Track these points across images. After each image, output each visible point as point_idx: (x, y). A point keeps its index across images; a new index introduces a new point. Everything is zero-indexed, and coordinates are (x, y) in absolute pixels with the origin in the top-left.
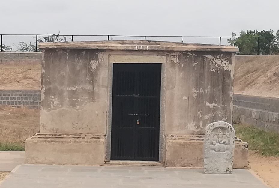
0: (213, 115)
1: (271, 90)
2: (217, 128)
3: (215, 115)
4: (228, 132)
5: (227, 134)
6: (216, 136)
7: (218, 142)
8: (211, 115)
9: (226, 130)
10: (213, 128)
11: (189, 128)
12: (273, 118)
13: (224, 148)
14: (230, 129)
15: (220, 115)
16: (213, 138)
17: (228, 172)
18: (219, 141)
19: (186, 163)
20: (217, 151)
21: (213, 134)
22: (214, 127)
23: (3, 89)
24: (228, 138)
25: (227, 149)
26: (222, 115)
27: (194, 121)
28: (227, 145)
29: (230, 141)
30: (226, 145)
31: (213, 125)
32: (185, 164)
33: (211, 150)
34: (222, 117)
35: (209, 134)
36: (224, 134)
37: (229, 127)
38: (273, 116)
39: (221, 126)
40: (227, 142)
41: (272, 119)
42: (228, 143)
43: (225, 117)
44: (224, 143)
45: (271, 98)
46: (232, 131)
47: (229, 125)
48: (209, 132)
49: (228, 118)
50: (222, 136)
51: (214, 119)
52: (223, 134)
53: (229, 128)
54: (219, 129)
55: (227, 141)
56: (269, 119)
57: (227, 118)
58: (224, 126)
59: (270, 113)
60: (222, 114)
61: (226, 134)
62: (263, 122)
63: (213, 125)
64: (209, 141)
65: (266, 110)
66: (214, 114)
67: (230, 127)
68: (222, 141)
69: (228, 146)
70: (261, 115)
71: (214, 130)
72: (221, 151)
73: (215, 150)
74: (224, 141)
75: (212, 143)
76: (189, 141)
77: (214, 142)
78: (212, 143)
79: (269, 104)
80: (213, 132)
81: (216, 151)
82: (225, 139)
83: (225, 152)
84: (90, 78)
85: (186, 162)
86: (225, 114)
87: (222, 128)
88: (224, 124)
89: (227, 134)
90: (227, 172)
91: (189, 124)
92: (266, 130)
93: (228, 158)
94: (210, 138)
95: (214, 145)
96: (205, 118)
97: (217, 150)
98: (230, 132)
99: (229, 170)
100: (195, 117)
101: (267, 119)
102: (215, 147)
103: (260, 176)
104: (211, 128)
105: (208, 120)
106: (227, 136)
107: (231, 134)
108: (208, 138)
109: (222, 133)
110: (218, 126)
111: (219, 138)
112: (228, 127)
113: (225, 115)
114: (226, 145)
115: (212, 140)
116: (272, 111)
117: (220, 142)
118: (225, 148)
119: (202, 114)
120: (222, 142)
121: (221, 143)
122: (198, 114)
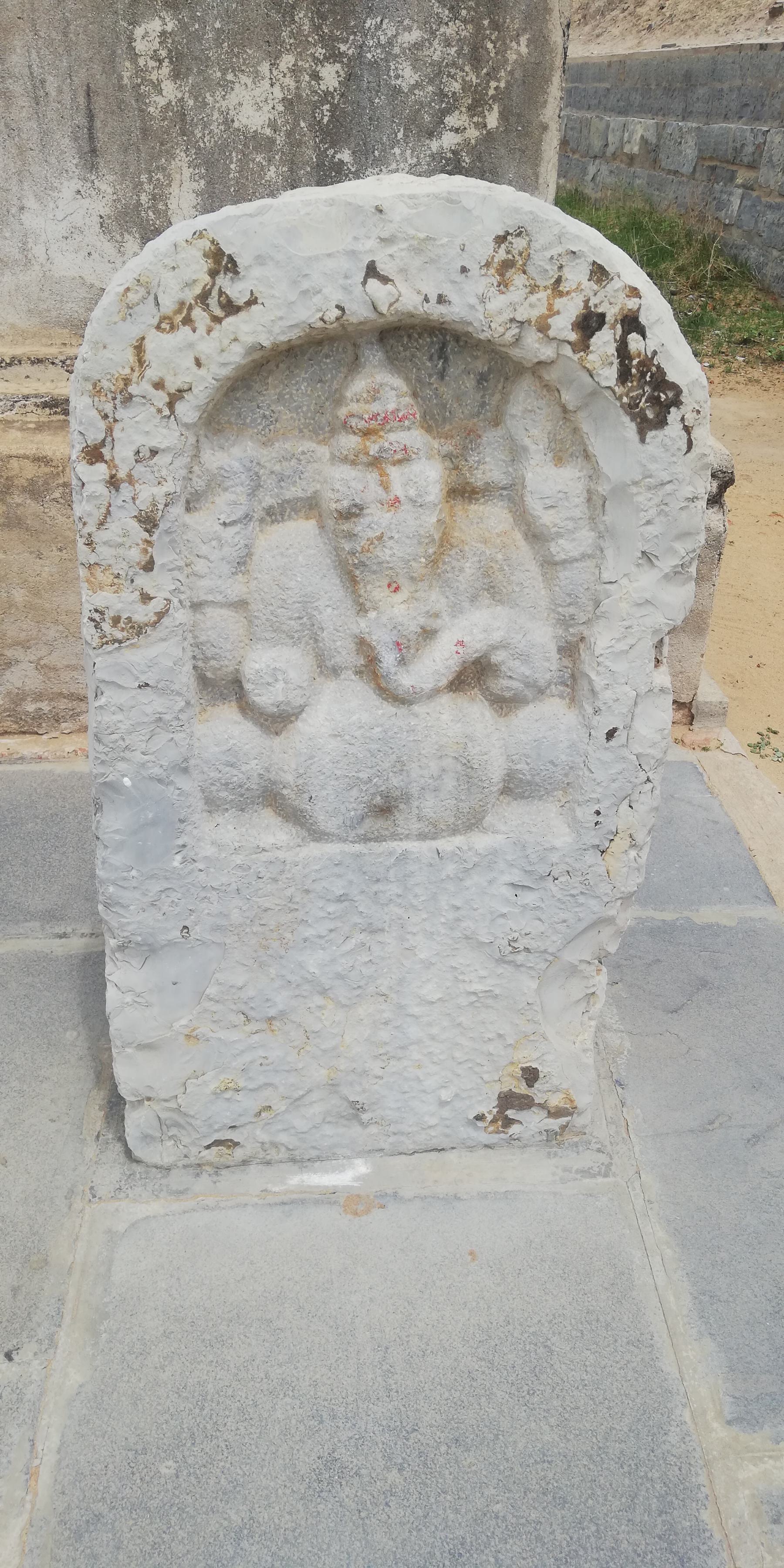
0: (331, 76)
1: (601, 38)
2: (322, 350)
3: (350, 78)
4: (570, 446)
5: (551, 483)
6: (301, 531)
7: (346, 654)
8: (295, 71)
10: (224, 347)
11: (38, 251)
12: (626, 139)
14: (609, 375)
15: (408, 76)
16: (236, 589)
17: (531, 1122)
18: (363, 644)
19: (39, 697)
20: (329, 824)
21: (225, 503)
22: (256, 329)
23: (83, 99)
24: (549, 564)
25: (514, 787)
26: (439, 71)
27: (91, 155)
28: (525, 716)
29: (602, 639)
30: (505, 704)
32: (31, 707)
33: (213, 805)
34: (441, 94)
35: (148, 493)
36: (478, 478)
37: (589, 323)
38: (626, 135)
40: (524, 657)
41: (622, 147)
42: (546, 664)
43: (476, 107)
44: (474, 674)
45: (615, 59)
47: (599, 273)
48: (122, 453)
49: (504, 116)
50: (442, 546)
51: (333, 133)
52: (462, 492)
53: (604, 341)
54: (359, 385)
55: (522, 633)
56: (606, 145)
57: (492, 120)
58: (481, 306)
59: (615, 121)
60: (436, 52)
61: (512, 493)
62: (576, 156)
63: (222, 262)
65: (589, 108)
66: (334, 56)
67: (631, 323)
68: (428, 634)
69: (548, 723)
70: (572, 129)
71: (270, 393)
72: (406, 821)
73: (294, 816)
74: (476, 645)
75: (224, 687)
76: (31, 449)
77: (273, 668)
78: (224, 687)
79: (608, 85)
80: (228, 457)
81: (318, 835)
82: (492, 588)
83: (481, 841)
85: (33, 681)
86: (476, 58)
87: (423, 343)
89: (551, 483)
90: (509, 1122)
91: (31, 202)
92: (589, 190)
93: (536, 927)
94: (159, 584)
95: (276, 721)
96: (228, 122)
97: (329, 806)
98: (615, 442)
99: (538, 1093)
100: (99, 103)
101: (597, 144)
104: (159, 345)
105: (263, 144)
107: (621, 491)
109: (427, 475)
111: (378, 592)
112: (563, 325)
113: (473, 78)
114: (505, 704)
115: (221, 626)
116: (623, 112)
117: (388, 659)
118: (496, 772)
119: (181, 61)
120: (438, 661)
122: (134, 57)
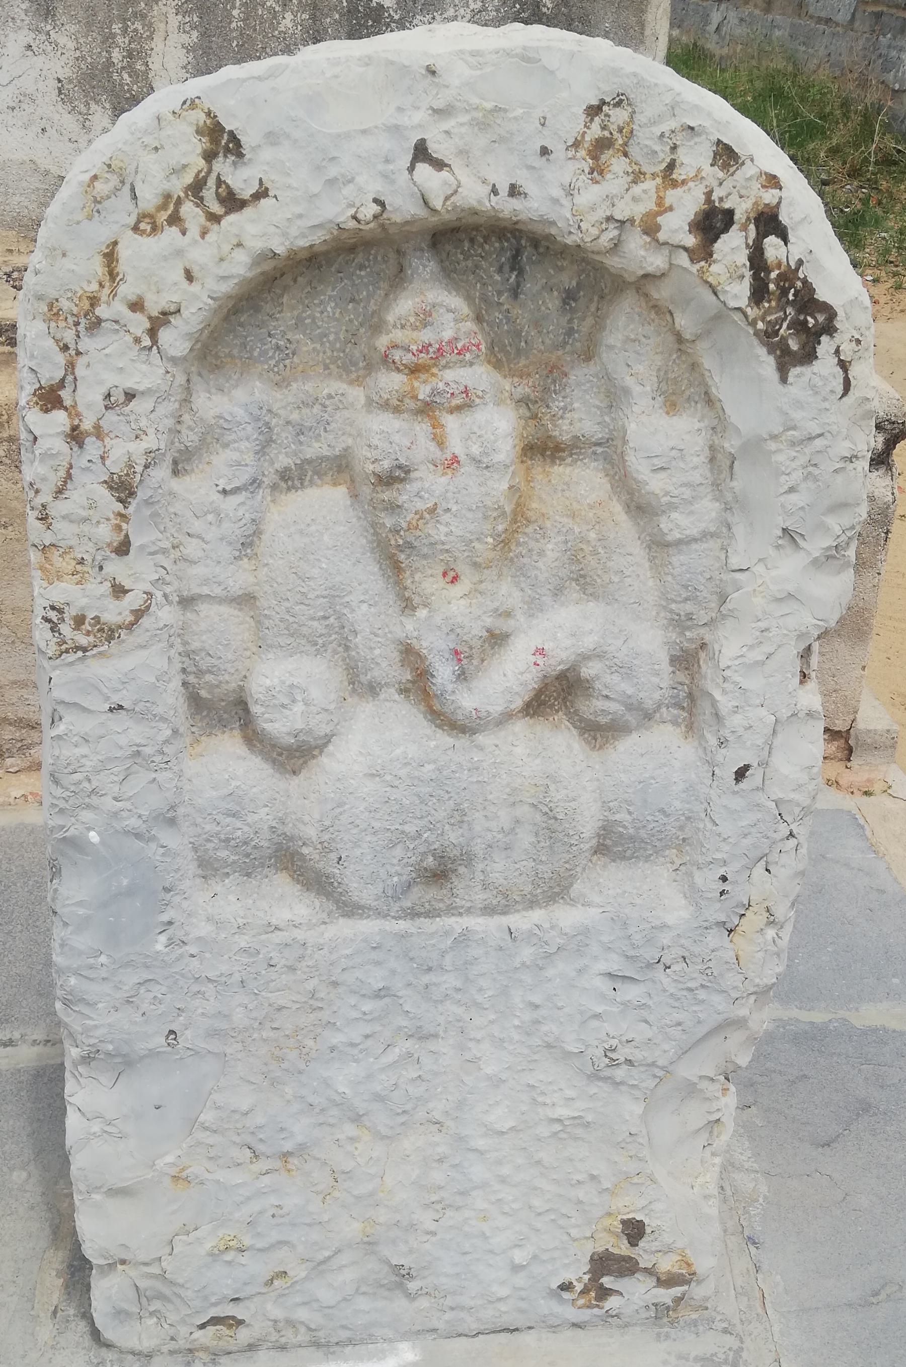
2: (354, 260)
4: (687, 387)
5: (660, 437)
6: (326, 501)
7: (387, 667)
9: (624, 325)
10: (223, 255)
13: (551, 825)
14: (739, 293)
16: (239, 578)
17: (635, 1293)
18: (409, 654)
20: (366, 895)
21: (225, 464)
22: (265, 231)
24: (659, 545)
29: (730, 646)
31: (189, 151)
33: (209, 868)
35: (122, 450)
36: (564, 431)
37: (712, 223)
39: (469, 185)
40: (626, 671)
42: (655, 680)
44: (558, 694)
46: (787, 359)
47: (726, 156)
48: (88, 398)
50: (515, 523)
52: (542, 449)
53: (733, 247)
54: (405, 306)
55: (624, 639)
58: (568, 200)
61: (610, 451)
63: (221, 141)
64: (142, 666)
67: (769, 222)
68: (497, 639)
69: (657, 758)
71: (285, 316)
72: (467, 889)
73: (317, 883)
74: (561, 654)
75: (224, 710)
77: (289, 684)
78: (224, 710)
80: (230, 402)
81: (350, 909)
82: (582, 578)
83: (567, 917)
84: (230, 355)
87: (488, 248)
88: (572, 123)
89: (660, 437)
90: (604, 1293)
94: (137, 572)
98: (749, 386)
99: (644, 1254)
102: (301, 804)
103: (278, 276)
104: (135, 251)
106: (641, 508)
107: (755, 447)
108: (87, 596)
109: (496, 426)
110: (367, 185)
111: (429, 583)
112: (677, 226)
115: (220, 630)
117: (443, 673)
120: (510, 676)
121: (467, 701)
